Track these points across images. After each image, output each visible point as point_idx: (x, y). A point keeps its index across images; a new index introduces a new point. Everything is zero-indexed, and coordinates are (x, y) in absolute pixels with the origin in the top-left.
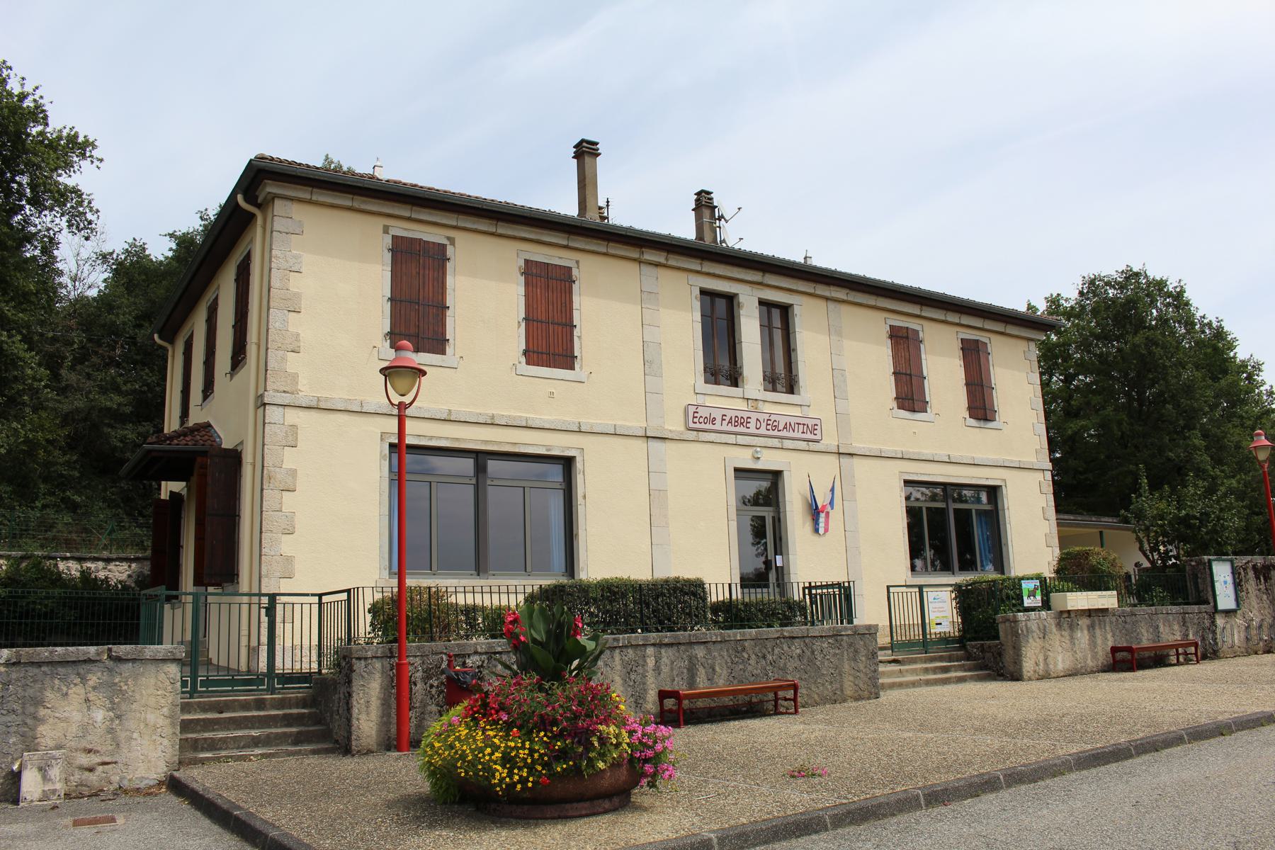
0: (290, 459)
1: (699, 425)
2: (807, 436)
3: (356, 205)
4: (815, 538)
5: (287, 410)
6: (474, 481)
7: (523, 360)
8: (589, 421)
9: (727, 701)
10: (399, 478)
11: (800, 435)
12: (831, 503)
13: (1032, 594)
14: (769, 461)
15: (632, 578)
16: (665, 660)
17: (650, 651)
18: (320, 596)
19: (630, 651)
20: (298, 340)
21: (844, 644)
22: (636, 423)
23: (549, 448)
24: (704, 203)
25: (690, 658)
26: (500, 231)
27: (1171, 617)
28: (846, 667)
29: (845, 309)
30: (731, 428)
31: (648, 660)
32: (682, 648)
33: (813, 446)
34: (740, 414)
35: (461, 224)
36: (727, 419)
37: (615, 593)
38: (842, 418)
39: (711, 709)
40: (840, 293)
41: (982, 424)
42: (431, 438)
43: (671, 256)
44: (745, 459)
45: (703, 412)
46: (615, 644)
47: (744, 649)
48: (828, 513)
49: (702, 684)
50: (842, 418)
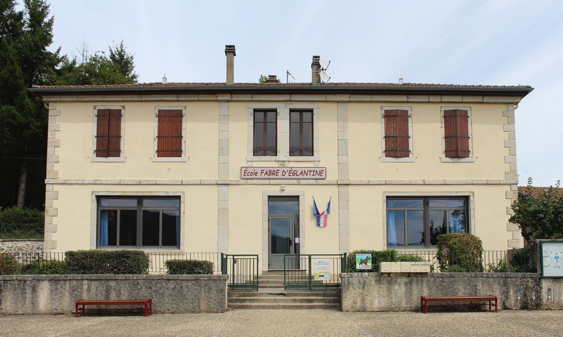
0: (55, 204)
1: (248, 175)
2: (318, 176)
3: (79, 99)
5: (54, 186)
6: (423, 209)
7: (384, 155)
8: (186, 179)
9: (127, 307)
10: (271, 209)
12: (328, 210)
13: (364, 262)
14: (290, 191)
16: (93, 286)
17: (85, 282)
18: (233, 256)
19: (75, 282)
20: (58, 158)
21: (203, 285)
23: (167, 192)
24: (316, 64)
25: (107, 286)
26: (143, 99)
27: (491, 280)
28: (203, 295)
29: (350, 105)
30: (266, 176)
31: (84, 286)
32: (103, 281)
35: (125, 99)
36: (265, 172)
37: (87, 257)
38: (343, 167)
39: (118, 310)
40: (345, 98)
41: (456, 160)
42: (113, 192)
43: (409, 96)
44: (275, 191)
45: (250, 170)
46: (66, 278)
47: (138, 284)
48: (326, 216)
49: (113, 297)
50: (343, 167)
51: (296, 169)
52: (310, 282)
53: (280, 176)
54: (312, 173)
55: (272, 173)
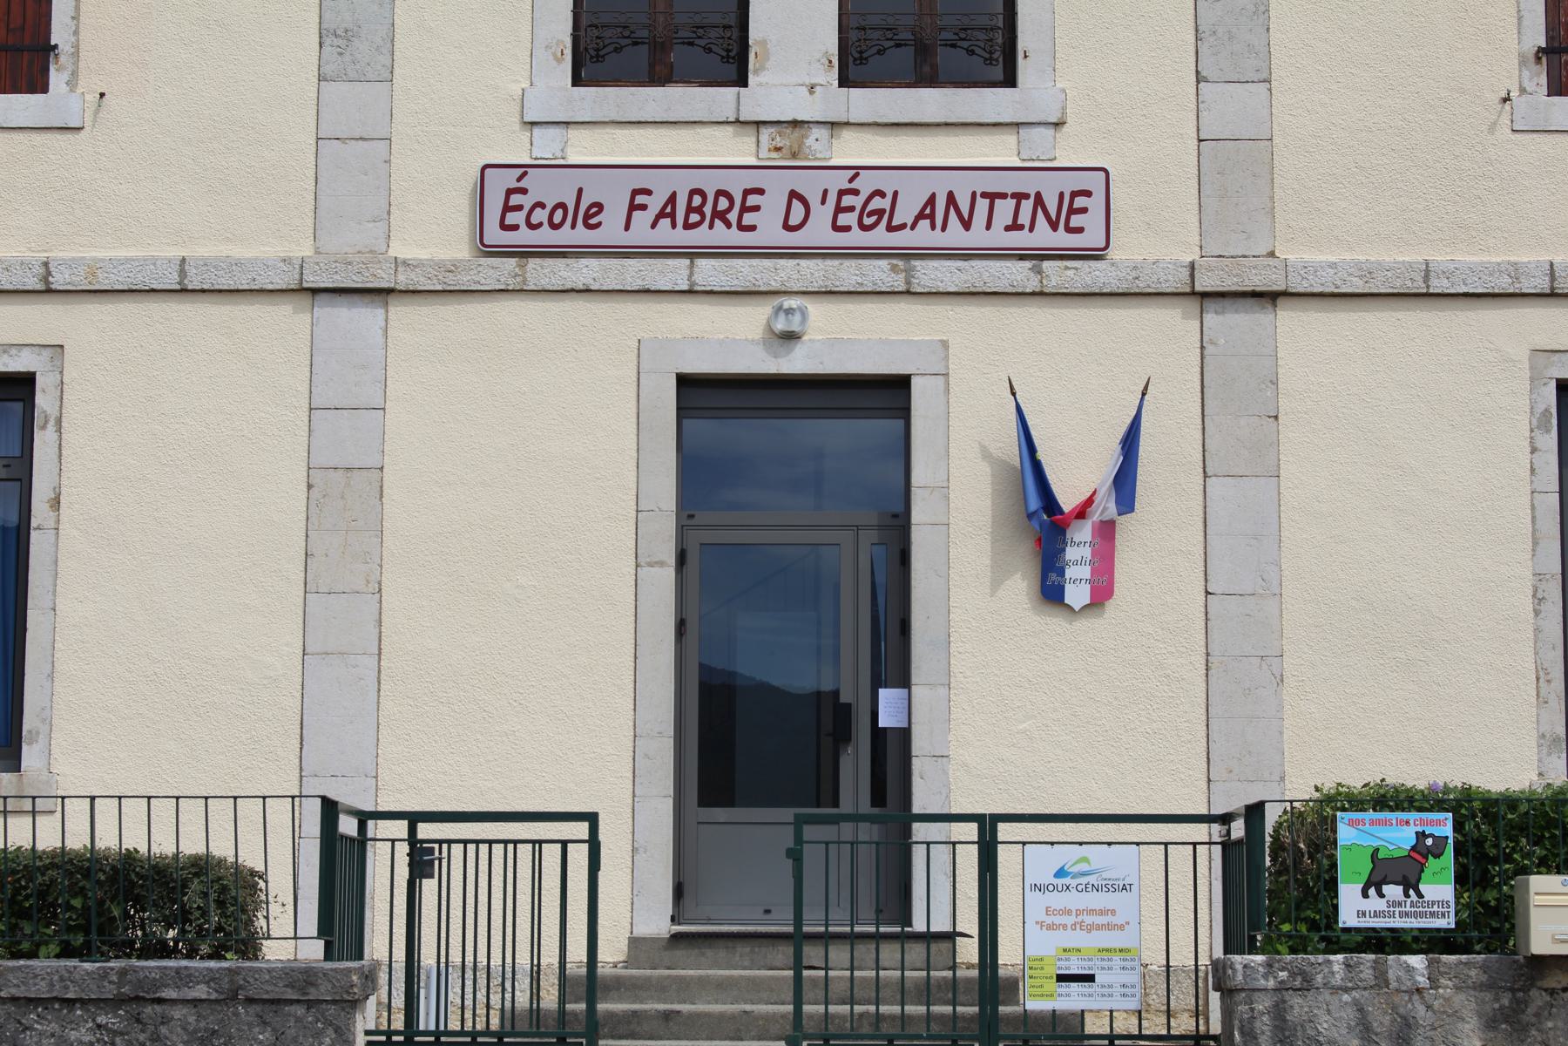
1: (530, 227)
2: (1051, 233)
4: (1053, 623)
11: (999, 237)
12: (1124, 482)
13: (1397, 872)
15: (1391, 781)
22: (278, 243)
30: (666, 234)
33: (1057, 275)
34: (710, 182)
36: (655, 203)
38: (1231, 163)
44: (732, 341)
45: (543, 188)
50: (1231, 163)
51: (887, 182)
52: (989, 1023)
53: (768, 228)
54: (1004, 209)
55: (711, 206)
